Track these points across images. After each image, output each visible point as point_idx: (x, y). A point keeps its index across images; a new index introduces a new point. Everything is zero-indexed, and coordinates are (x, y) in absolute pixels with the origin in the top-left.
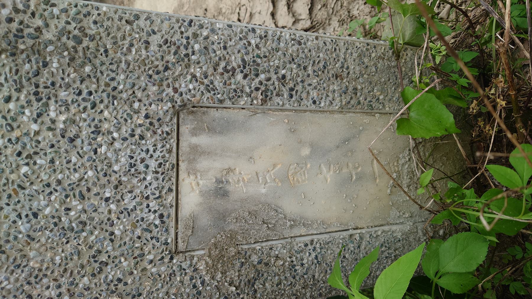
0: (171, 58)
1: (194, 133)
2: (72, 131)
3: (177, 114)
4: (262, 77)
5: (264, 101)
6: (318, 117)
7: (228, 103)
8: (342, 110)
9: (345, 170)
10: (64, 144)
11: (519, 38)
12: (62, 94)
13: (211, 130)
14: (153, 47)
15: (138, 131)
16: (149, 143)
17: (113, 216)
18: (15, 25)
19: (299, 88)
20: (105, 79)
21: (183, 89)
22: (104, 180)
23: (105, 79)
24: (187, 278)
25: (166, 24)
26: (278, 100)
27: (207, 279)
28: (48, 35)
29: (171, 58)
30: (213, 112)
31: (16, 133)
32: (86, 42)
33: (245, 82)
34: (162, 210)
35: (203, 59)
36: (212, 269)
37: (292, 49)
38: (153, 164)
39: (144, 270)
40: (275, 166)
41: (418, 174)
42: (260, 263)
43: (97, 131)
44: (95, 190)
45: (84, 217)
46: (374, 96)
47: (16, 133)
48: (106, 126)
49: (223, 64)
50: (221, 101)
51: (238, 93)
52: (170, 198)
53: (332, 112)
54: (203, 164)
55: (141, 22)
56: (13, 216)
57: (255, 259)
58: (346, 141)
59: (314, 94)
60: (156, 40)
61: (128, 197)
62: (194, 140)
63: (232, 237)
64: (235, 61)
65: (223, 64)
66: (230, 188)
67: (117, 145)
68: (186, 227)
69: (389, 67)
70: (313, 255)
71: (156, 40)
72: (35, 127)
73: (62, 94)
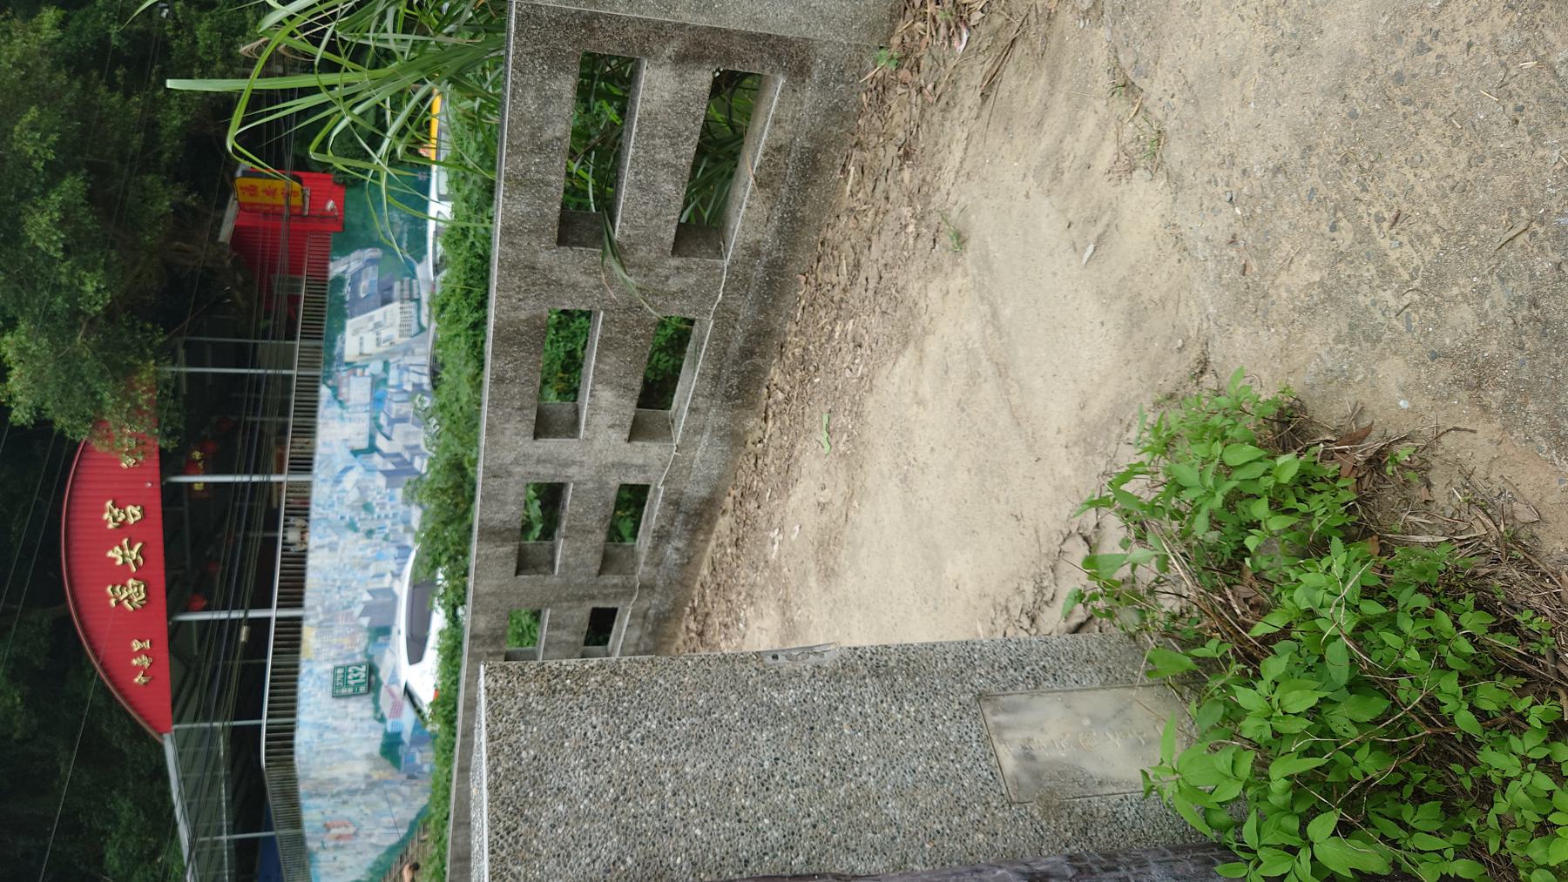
0: (963, 665)
1: (994, 713)
2: (920, 717)
3: (978, 700)
4: (1028, 668)
5: (1037, 685)
6: (1085, 694)
7: (1010, 691)
8: (1104, 686)
9: (1130, 736)
10: (918, 725)
11: (394, 117)
12: (908, 695)
13: (1005, 711)
14: (949, 661)
15: (957, 714)
16: (966, 721)
17: (960, 773)
18: (874, 661)
19: (1060, 673)
20: (928, 684)
21: (976, 683)
22: (947, 748)
23: (928, 684)
24: (1028, 823)
25: (953, 647)
26: (1046, 683)
27: (1044, 823)
28: (891, 664)
29: (963, 665)
30: (1001, 698)
31: (891, 721)
32: (912, 664)
33: (1016, 674)
34: (990, 769)
35: (982, 663)
36: (1044, 815)
37: (1043, 648)
38: (974, 736)
39: (993, 814)
40: (1064, 735)
41: (669, 51)
42: (1084, 813)
43: (934, 716)
44: (943, 754)
45: (942, 773)
46: (1128, 673)
47: (891, 721)
48: (937, 712)
49: (997, 665)
50: (1005, 689)
51: (1014, 683)
52: (993, 760)
53: (1096, 689)
54: (1008, 735)
55: (938, 648)
56: (902, 772)
57: (1078, 810)
58: (1120, 711)
59: (1074, 676)
60: (949, 656)
61: (965, 759)
62: (996, 719)
63: (1051, 792)
64: (1004, 661)
65: (997, 665)
66: (1035, 753)
67: (948, 724)
68: (1012, 782)
69: (1131, 649)
70: (1133, 809)
71: (949, 656)
72: (899, 716)
73: (908, 695)
